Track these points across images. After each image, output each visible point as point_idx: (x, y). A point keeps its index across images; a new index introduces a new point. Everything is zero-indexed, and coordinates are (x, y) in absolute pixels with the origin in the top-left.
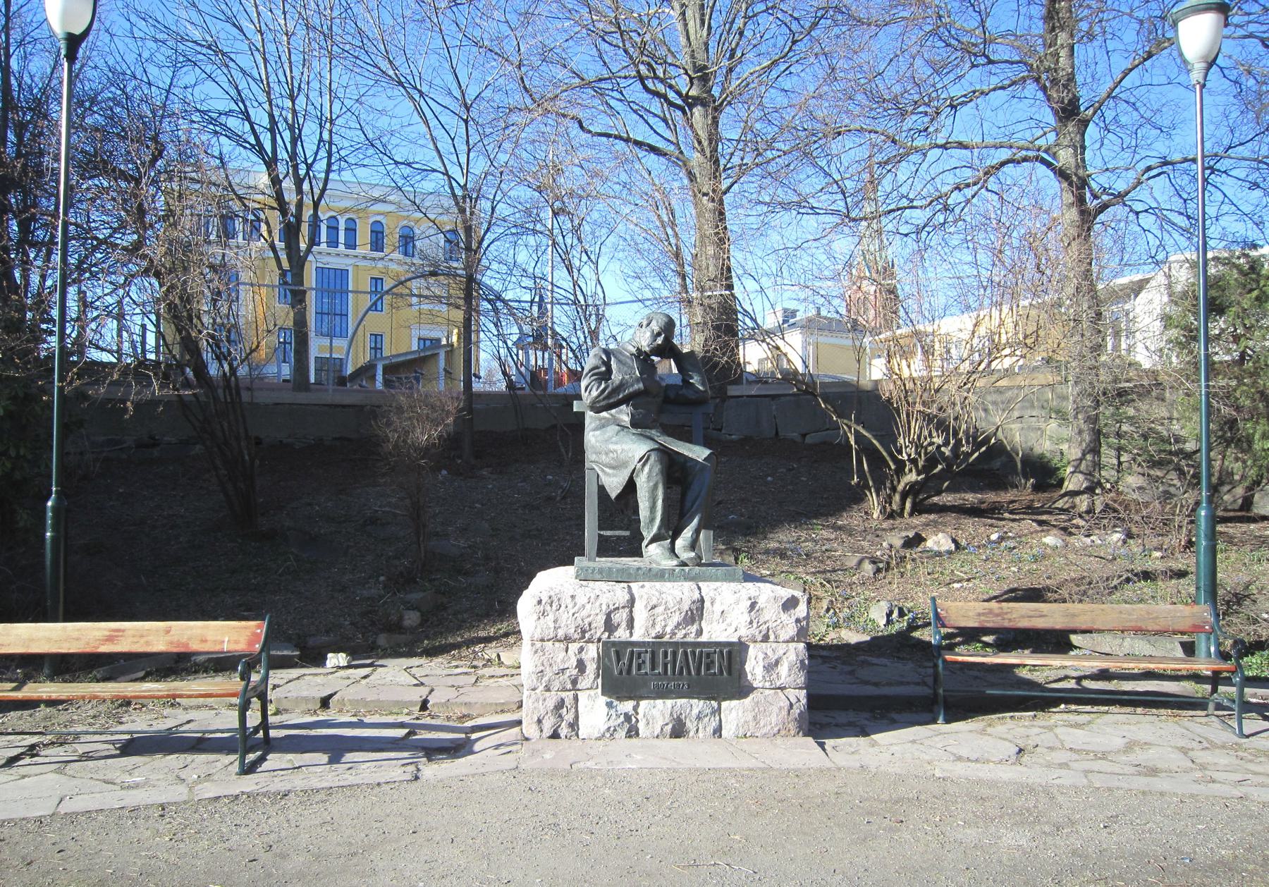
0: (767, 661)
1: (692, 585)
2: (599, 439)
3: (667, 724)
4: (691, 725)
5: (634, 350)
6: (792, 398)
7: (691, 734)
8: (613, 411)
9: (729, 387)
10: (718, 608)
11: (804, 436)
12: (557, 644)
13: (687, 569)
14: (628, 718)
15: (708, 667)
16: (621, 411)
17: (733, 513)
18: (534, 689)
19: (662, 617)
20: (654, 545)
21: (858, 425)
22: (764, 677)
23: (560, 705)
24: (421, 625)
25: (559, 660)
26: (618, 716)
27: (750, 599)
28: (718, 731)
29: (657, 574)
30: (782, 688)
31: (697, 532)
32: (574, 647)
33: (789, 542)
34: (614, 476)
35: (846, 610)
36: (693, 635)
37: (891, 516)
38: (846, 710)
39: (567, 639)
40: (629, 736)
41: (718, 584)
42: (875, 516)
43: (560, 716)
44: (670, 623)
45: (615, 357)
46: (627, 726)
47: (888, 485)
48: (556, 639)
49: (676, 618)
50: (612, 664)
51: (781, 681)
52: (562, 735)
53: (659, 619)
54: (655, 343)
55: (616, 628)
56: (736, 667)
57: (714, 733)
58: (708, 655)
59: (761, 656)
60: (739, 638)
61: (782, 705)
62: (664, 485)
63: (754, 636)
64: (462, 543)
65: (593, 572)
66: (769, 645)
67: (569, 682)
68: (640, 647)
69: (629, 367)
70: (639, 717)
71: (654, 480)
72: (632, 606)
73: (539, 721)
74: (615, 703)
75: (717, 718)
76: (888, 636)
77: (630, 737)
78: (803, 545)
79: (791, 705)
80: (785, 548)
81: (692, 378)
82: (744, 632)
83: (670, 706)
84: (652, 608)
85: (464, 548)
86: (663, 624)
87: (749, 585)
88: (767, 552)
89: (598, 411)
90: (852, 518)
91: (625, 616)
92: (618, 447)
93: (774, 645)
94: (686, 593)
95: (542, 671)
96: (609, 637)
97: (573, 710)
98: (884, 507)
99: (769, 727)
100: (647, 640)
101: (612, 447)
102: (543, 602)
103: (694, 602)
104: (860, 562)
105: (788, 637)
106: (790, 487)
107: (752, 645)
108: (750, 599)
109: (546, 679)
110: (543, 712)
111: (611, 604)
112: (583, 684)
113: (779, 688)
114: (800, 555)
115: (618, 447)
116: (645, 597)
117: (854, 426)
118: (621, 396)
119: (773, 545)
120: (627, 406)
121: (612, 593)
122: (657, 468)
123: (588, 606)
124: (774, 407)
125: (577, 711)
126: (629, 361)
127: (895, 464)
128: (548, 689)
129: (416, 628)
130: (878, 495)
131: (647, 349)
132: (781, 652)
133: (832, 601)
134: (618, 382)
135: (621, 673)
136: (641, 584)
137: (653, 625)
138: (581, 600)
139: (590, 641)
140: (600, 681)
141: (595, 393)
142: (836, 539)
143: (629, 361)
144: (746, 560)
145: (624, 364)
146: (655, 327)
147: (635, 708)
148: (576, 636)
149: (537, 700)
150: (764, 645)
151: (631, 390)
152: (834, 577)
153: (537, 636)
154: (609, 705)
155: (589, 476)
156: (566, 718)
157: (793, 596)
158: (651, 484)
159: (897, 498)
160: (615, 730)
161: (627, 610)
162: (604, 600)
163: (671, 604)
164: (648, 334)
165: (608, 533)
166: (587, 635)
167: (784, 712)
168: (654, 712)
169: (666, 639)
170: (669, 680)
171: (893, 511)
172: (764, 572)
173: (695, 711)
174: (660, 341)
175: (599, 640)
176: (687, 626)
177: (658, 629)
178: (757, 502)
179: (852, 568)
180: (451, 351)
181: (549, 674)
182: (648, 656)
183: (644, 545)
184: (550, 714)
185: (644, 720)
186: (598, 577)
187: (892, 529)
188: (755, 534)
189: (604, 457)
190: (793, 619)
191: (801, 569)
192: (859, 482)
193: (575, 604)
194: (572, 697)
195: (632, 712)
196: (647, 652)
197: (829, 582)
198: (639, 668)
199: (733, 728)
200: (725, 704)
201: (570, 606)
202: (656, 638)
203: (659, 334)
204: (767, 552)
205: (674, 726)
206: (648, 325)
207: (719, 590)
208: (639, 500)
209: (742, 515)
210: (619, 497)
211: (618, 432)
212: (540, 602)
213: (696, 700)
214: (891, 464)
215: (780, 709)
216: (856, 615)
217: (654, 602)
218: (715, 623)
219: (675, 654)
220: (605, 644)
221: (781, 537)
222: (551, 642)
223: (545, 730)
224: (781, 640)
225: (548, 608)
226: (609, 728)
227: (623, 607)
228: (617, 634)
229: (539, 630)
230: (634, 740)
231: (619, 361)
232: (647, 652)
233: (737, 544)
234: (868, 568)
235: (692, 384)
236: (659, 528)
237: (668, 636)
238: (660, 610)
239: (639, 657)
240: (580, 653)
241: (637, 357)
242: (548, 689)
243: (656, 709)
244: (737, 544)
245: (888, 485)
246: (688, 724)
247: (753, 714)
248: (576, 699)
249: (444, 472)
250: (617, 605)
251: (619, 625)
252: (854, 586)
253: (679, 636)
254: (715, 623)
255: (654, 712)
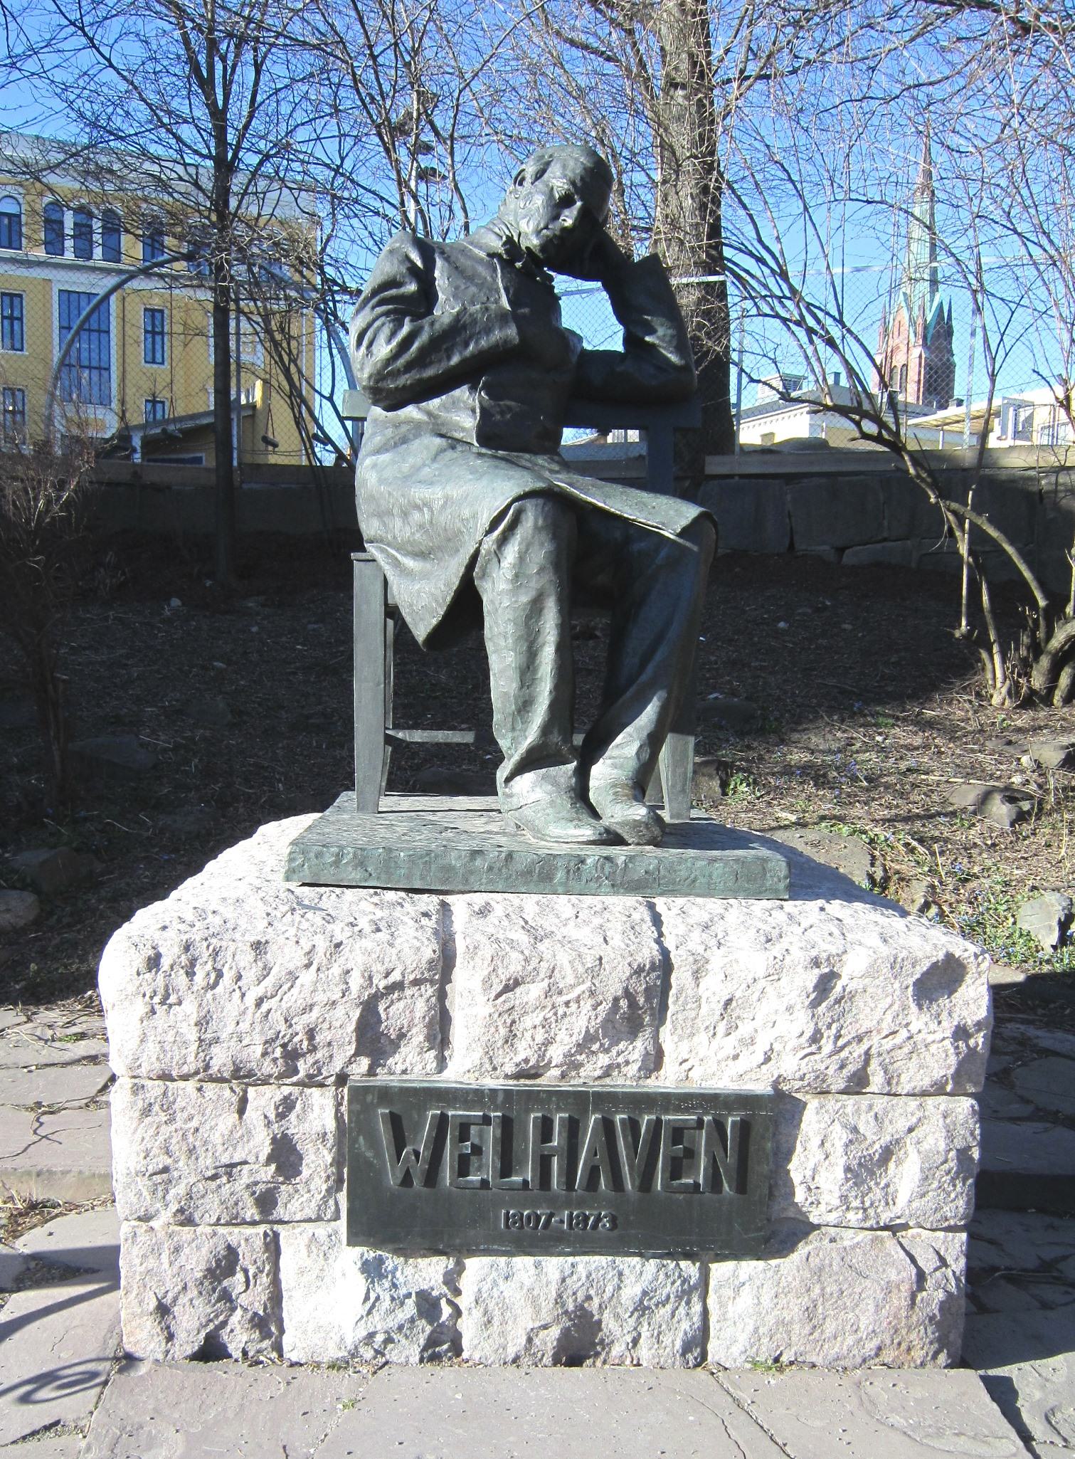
0: (856, 1151)
1: (625, 905)
2: (388, 473)
3: (545, 1327)
4: (615, 1327)
5: (497, 245)
6: (823, 480)
7: (617, 1350)
8: (434, 403)
9: (709, 459)
10: (713, 989)
11: (841, 551)
12: (210, 1089)
13: (619, 853)
14: (427, 1305)
15: (676, 1170)
16: (454, 403)
17: (714, 689)
18: (146, 1218)
19: (537, 1018)
20: (528, 778)
21: (980, 514)
22: (844, 1198)
23: (227, 1263)
24: (37, 924)
25: (216, 1138)
26: (399, 1302)
27: (816, 963)
28: (697, 1345)
29: (529, 872)
30: (893, 1229)
31: (654, 742)
32: (263, 1100)
33: (830, 752)
34: (425, 576)
35: (963, 907)
36: (633, 1069)
37: (1029, 701)
38: (1021, 1209)
39: (242, 1075)
40: (431, 1355)
41: (714, 905)
42: (996, 700)
43: (226, 1296)
44: (562, 1036)
45: (447, 259)
46: (424, 1329)
47: (1025, 639)
48: (205, 1075)
49: (582, 1021)
50: (379, 1154)
51: (896, 1210)
52: (234, 1348)
53: (528, 1021)
54: (556, 227)
55: (395, 1045)
56: (758, 1169)
57: (686, 1349)
58: (678, 1133)
59: (839, 1136)
60: (776, 1084)
61: (893, 1276)
62: (560, 601)
63: (821, 1077)
64: (163, 741)
65: (337, 863)
66: (864, 1101)
67: (249, 1201)
68: (468, 1105)
69: (481, 286)
70: (464, 1302)
71: (534, 585)
72: (446, 977)
73: (163, 1310)
74: (391, 1261)
75: (697, 1308)
76: (1064, 974)
77: (436, 1358)
78: (862, 757)
79: (921, 1276)
80: (824, 765)
81: (652, 331)
82: (790, 1065)
83: (555, 1276)
84: (507, 989)
85: (165, 750)
86: (540, 1037)
87: (809, 909)
88: (788, 771)
89: (394, 401)
90: (959, 709)
91: (421, 1007)
92: (435, 494)
93: (880, 1103)
94: (617, 940)
95: (165, 1170)
96: (371, 1072)
97: (265, 1280)
98: (1017, 685)
99: (850, 1340)
100: (490, 1083)
101: (419, 493)
102: (165, 963)
103: (639, 971)
104: (985, 798)
105: (926, 1083)
106: (822, 642)
107: (813, 1104)
108: (816, 963)
109: (179, 1190)
110: (172, 1286)
111: (378, 969)
112: (294, 1205)
113: (886, 1228)
114: (855, 779)
115: (435, 494)
116: (487, 951)
117: (970, 517)
118: (455, 360)
119: (798, 757)
120: (473, 388)
121: (383, 936)
122: (540, 554)
123: (307, 977)
124: (789, 497)
125: (276, 1282)
126: (483, 271)
127: (1047, 595)
128: (186, 1219)
129: (23, 931)
130: (1004, 661)
131: (533, 242)
132: (902, 1125)
133: (933, 887)
134: (446, 320)
135: (407, 1180)
136: (479, 899)
137: (511, 1038)
138: (285, 957)
139: (312, 1081)
140: (343, 1197)
141: (383, 349)
142: (926, 747)
143: (483, 271)
144: (743, 788)
145: (470, 278)
146: (558, 182)
147: (451, 1280)
148: (268, 1068)
149: (156, 1250)
150: (850, 1101)
151: (483, 343)
152: (930, 830)
153: (150, 1064)
154: (372, 1270)
155: (362, 575)
156: (243, 1300)
157: (949, 957)
158: (525, 598)
159: (1045, 662)
160: (389, 1340)
161: (429, 990)
162: (357, 957)
163: (567, 977)
164: (539, 200)
165: (417, 736)
166: (303, 1067)
167: (900, 1300)
168: (510, 1290)
169: (550, 1079)
170: (555, 1204)
171: (1032, 692)
172: (783, 815)
173: (631, 1291)
174: (568, 219)
175: (342, 1079)
176: (615, 1042)
177: (524, 1051)
178: (762, 668)
179: (964, 810)
180: (253, 416)
181: (186, 1176)
182: (492, 1132)
183: (502, 773)
184: (193, 1292)
185: (477, 1313)
186: (355, 876)
187: (1036, 729)
188: (762, 732)
189: (398, 523)
190: (948, 1027)
191: (858, 810)
192: (970, 632)
193: (267, 971)
194: (259, 1243)
195: (439, 1289)
196: (486, 1120)
197: (921, 841)
198: (463, 1167)
199: (743, 1339)
200: (721, 1271)
201: (249, 976)
202: (517, 1076)
203: (566, 201)
204: (788, 771)
205: (566, 1333)
206: (540, 175)
207: (719, 928)
208: (490, 647)
209: (734, 693)
210: (436, 635)
211: (442, 451)
212: (154, 962)
213: (635, 1260)
214: (1038, 595)
215: (889, 1289)
216: (989, 920)
217: (514, 966)
218: (703, 1037)
219: (574, 1129)
220: (359, 1094)
221: (815, 740)
222: (191, 1085)
223: (181, 1336)
224: (905, 1087)
225: (180, 979)
226: (371, 1336)
227: (416, 983)
228: (396, 1062)
229: (152, 1048)
230: (445, 1373)
231: (456, 270)
232: (486, 1120)
233: (725, 754)
234: (1001, 811)
235: (652, 346)
236: (546, 730)
237: (555, 1072)
238: (532, 992)
239: (464, 1134)
240: (281, 1116)
241: (507, 264)
242: (186, 1219)
243: (513, 1284)
244: (725, 754)
245: (1025, 639)
246: (609, 1324)
247: (805, 1301)
248: (273, 1247)
249: (176, 602)
250: (395, 976)
251: (402, 1036)
252: (974, 852)
253: (589, 1074)
254: (703, 1037)
255: (510, 1290)
